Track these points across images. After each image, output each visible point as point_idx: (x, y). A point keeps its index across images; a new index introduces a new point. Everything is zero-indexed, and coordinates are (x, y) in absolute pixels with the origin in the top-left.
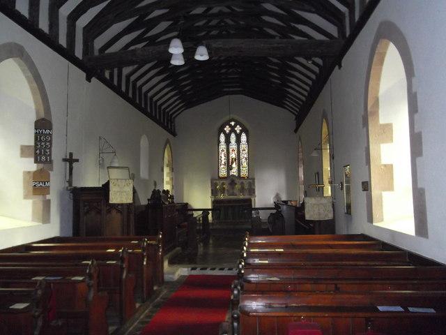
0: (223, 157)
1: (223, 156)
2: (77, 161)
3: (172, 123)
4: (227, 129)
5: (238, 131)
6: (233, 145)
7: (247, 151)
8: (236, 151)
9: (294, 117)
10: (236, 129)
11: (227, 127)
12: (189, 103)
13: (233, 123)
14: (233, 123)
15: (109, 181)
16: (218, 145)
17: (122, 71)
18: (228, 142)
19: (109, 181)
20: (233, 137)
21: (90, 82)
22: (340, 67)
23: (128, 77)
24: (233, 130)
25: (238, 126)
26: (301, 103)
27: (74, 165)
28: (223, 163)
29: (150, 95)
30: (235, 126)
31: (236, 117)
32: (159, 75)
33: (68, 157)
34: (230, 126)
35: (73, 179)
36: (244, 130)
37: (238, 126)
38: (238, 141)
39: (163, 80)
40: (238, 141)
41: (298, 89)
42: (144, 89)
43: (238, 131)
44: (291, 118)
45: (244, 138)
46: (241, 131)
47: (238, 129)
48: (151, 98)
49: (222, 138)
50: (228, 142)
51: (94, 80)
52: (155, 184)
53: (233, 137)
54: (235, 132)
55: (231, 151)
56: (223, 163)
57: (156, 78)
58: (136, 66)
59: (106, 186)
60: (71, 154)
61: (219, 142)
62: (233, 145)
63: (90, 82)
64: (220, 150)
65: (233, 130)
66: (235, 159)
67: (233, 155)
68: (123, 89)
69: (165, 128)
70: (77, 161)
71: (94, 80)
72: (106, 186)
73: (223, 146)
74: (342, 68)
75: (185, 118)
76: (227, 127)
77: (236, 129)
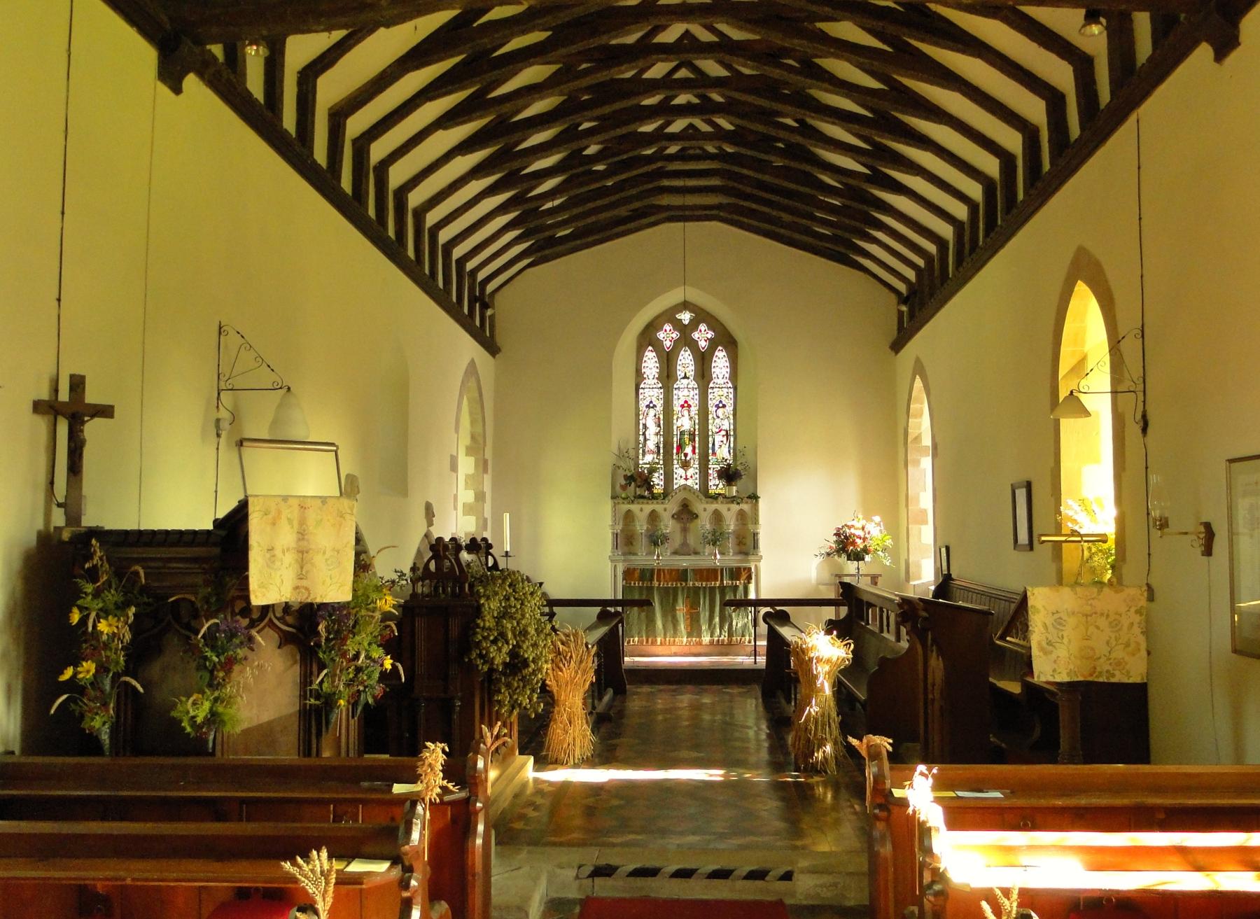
0: (652, 429)
1: (651, 422)
2: (105, 412)
3: (485, 306)
4: (667, 335)
5: (703, 344)
6: (686, 391)
7: (730, 409)
8: (694, 410)
9: (40, 525)
10: (696, 335)
11: (668, 327)
12: (544, 246)
13: (686, 317)
14: (686, 317)
15: (240, 515)
16: (637, 388)
17: (282, 53)
18: (668, 376)
19: (240, 515)
20: (686, 361)
21: (177, 90)
22: (1225, 44)
23: (339, 116)
24: (685, 339)
25: (703, 327)
26: (920, 262)
27: (93, 429)
28: (651, 445)
29: (415, 198)
30: (694, 325)
31: (695, 296)
32: (815, 876)
33: (64, 396)
34: (678, 325)
35: (86, 490)
36: (725, 339)
37: (703, 327)
38: (703, 374)
39: (476, 172)
40: (703, 374)
41: (933, 193)
42: (398, 174)
43: (703, 344)
44: (887, 310)
45: (720, 364)
46: (713, 344)
47: (703, 335)
48: (420, 213)
49: (651, 364)
50: (668, 376)
51: (191, 82)
52: (429, 512)
53: (686, 361)
54: (693, 345)
55: (677, 408)
56: (651, 445)
57: (440, 134)
58: (338, 35)
59: (233, 529)
60: (77, 384)
61: (639, 376)
62: (686, 391)
63: (177, 90)
64: (643, 405)
65: (685, 339)
66: (692, 436)
67: (684, 422)
68: (320, 154)
69: (466, 323)
70: (105, 412)
71: (191, 82)
72: (233, 529)
73: (652, 392)
74: (1233, 57)
75: (539, 295)
76: (668, 327)
77: (696, 335)
